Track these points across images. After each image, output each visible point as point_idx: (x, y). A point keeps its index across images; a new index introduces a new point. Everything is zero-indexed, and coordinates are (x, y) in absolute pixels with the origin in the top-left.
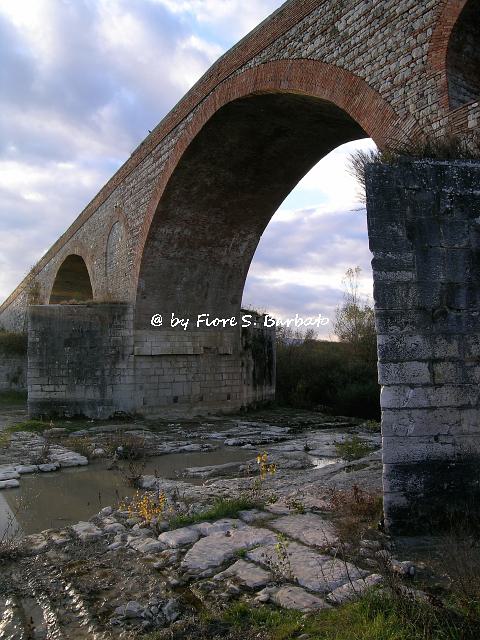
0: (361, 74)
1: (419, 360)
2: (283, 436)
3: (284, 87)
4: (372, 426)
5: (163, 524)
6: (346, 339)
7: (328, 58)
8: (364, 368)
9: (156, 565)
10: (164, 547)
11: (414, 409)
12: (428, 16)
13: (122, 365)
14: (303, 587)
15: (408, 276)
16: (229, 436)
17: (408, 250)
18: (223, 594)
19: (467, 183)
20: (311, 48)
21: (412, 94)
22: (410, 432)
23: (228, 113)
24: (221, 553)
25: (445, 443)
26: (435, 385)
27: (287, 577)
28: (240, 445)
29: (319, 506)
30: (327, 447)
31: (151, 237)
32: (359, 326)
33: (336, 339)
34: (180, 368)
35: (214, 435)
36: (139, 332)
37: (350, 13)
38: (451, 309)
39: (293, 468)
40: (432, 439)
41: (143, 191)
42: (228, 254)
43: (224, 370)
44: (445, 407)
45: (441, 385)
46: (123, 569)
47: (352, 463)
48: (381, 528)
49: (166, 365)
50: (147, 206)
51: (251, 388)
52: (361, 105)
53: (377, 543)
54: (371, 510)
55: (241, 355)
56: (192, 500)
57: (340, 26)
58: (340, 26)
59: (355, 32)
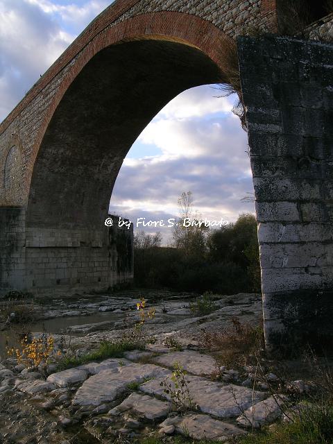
0: (209, 18)
1: (289, 201)
5: (52, 367)
7: (182, 9)
9: (44, 405)
10: (52, 387)
11: (287, 243)
13: (16, 255)
14: (207, 414)
15: (277, 128)
16: (101, 306)
17: (276, 108)
18: (122, 430)
22: (285, 264)
23: (103, 57)
24: (113, 388)
26: (303, 222)
27: (187, 405)
28: (111, 310)
31: (41, 155)
34: (61, 258)
35: (90, 305)
36: (30, 229)
40: (303, 271)
41: (35, 121)
42: (100, 172)
43: (95, 259)
45: (308, 223)
46: (8, 413)
48: (263, 354)
49: (51, 255)
50: (36, 132)
51: (116, 273)
52: (208, 42)
54: (252, 339)
55: (109, 248)
56: (77, 347)
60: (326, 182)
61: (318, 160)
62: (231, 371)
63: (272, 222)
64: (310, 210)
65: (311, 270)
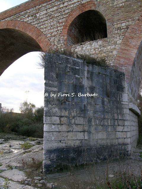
0: (42, 30)
1: (57, 116)
2: (2, 142)
3: (17, 29)
4: (31, 139)
6: (23, 113)
8: (28, 121)
12: (64, 19)
19: (74, 64)
20: (28, 19)
21: (57, 39)
25: (63, 143)
29: (18, 166)
30: (17, 146)
32: (27, 109)
33: (20, 112)
37: (41, 12)
38: (67, 101)
39: (6, 153)
40: (59, 142)
44: (63, 131)
47: (26, 150)
53: (40, 178)
57: (38, 15)
58: (38, 15)
59: (42, 18)
60: (71, 110)
61: (69, 102)
62: (29, 179)
63: (50, 124)
64: (64, 120)
65: (62, 142)
